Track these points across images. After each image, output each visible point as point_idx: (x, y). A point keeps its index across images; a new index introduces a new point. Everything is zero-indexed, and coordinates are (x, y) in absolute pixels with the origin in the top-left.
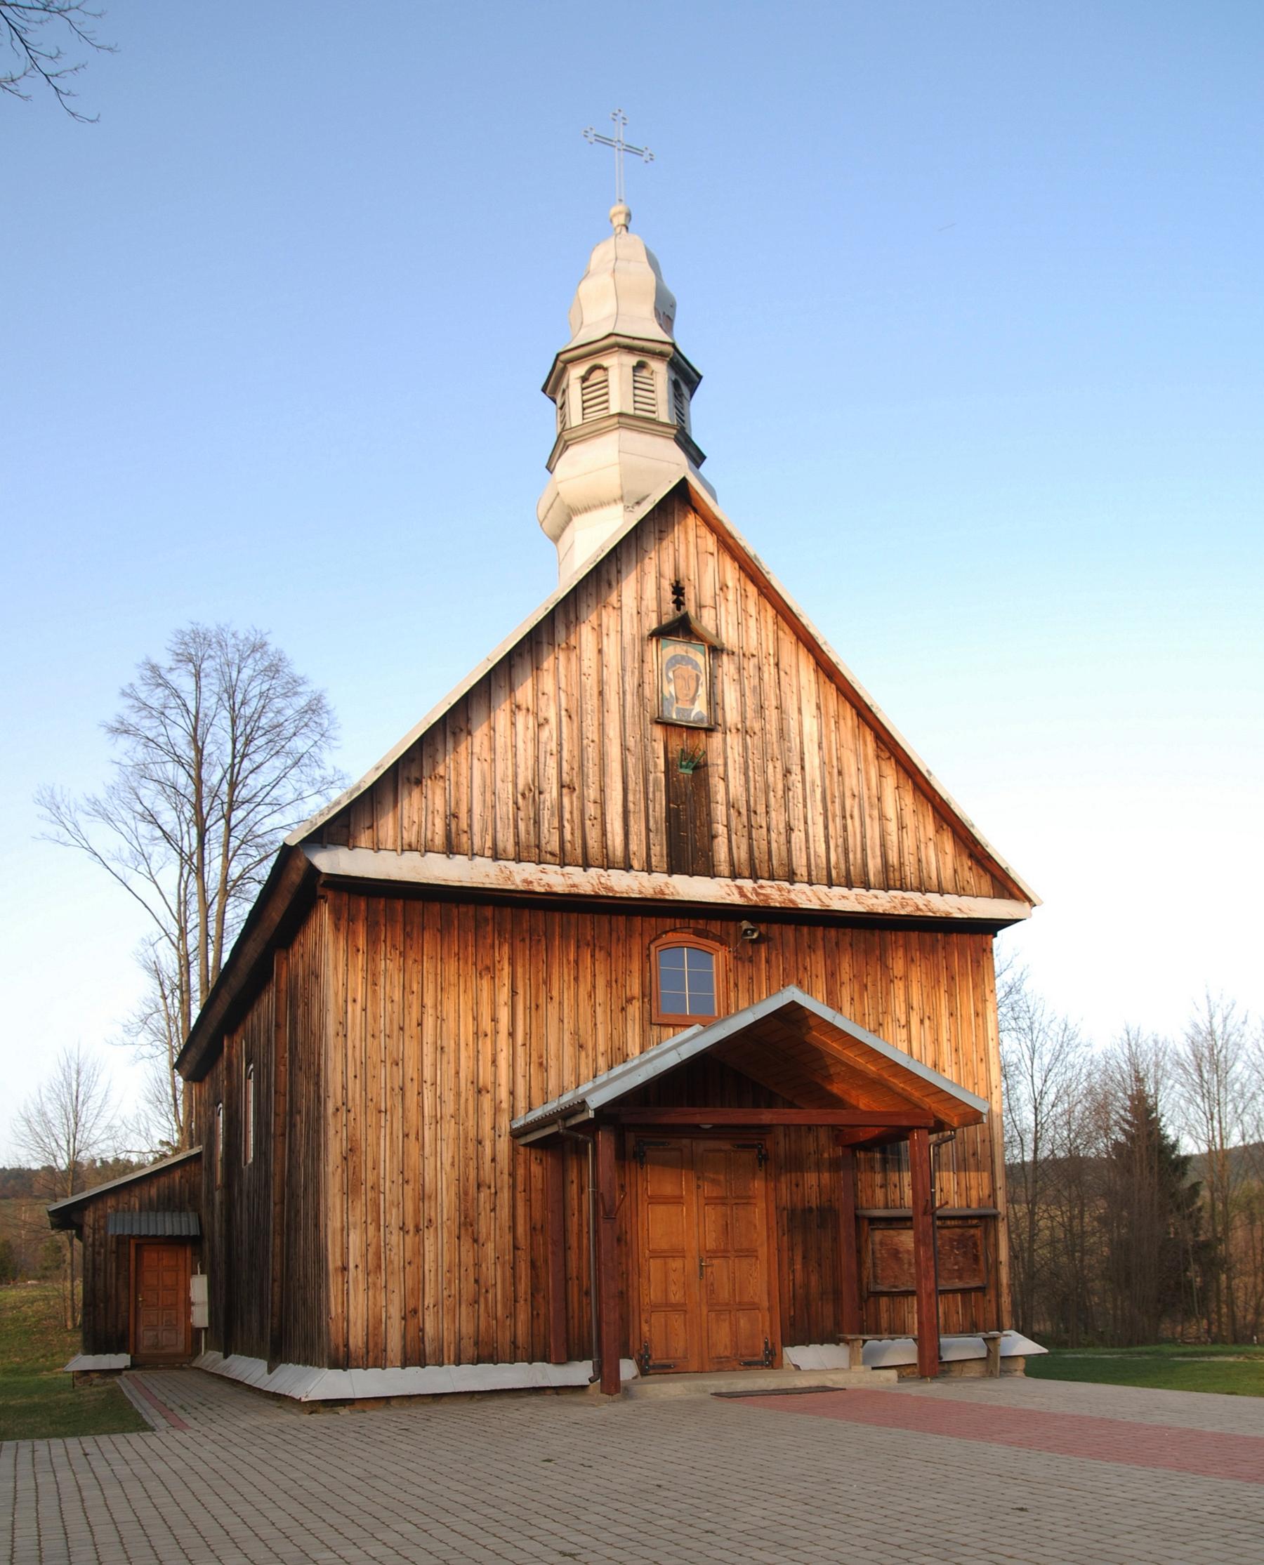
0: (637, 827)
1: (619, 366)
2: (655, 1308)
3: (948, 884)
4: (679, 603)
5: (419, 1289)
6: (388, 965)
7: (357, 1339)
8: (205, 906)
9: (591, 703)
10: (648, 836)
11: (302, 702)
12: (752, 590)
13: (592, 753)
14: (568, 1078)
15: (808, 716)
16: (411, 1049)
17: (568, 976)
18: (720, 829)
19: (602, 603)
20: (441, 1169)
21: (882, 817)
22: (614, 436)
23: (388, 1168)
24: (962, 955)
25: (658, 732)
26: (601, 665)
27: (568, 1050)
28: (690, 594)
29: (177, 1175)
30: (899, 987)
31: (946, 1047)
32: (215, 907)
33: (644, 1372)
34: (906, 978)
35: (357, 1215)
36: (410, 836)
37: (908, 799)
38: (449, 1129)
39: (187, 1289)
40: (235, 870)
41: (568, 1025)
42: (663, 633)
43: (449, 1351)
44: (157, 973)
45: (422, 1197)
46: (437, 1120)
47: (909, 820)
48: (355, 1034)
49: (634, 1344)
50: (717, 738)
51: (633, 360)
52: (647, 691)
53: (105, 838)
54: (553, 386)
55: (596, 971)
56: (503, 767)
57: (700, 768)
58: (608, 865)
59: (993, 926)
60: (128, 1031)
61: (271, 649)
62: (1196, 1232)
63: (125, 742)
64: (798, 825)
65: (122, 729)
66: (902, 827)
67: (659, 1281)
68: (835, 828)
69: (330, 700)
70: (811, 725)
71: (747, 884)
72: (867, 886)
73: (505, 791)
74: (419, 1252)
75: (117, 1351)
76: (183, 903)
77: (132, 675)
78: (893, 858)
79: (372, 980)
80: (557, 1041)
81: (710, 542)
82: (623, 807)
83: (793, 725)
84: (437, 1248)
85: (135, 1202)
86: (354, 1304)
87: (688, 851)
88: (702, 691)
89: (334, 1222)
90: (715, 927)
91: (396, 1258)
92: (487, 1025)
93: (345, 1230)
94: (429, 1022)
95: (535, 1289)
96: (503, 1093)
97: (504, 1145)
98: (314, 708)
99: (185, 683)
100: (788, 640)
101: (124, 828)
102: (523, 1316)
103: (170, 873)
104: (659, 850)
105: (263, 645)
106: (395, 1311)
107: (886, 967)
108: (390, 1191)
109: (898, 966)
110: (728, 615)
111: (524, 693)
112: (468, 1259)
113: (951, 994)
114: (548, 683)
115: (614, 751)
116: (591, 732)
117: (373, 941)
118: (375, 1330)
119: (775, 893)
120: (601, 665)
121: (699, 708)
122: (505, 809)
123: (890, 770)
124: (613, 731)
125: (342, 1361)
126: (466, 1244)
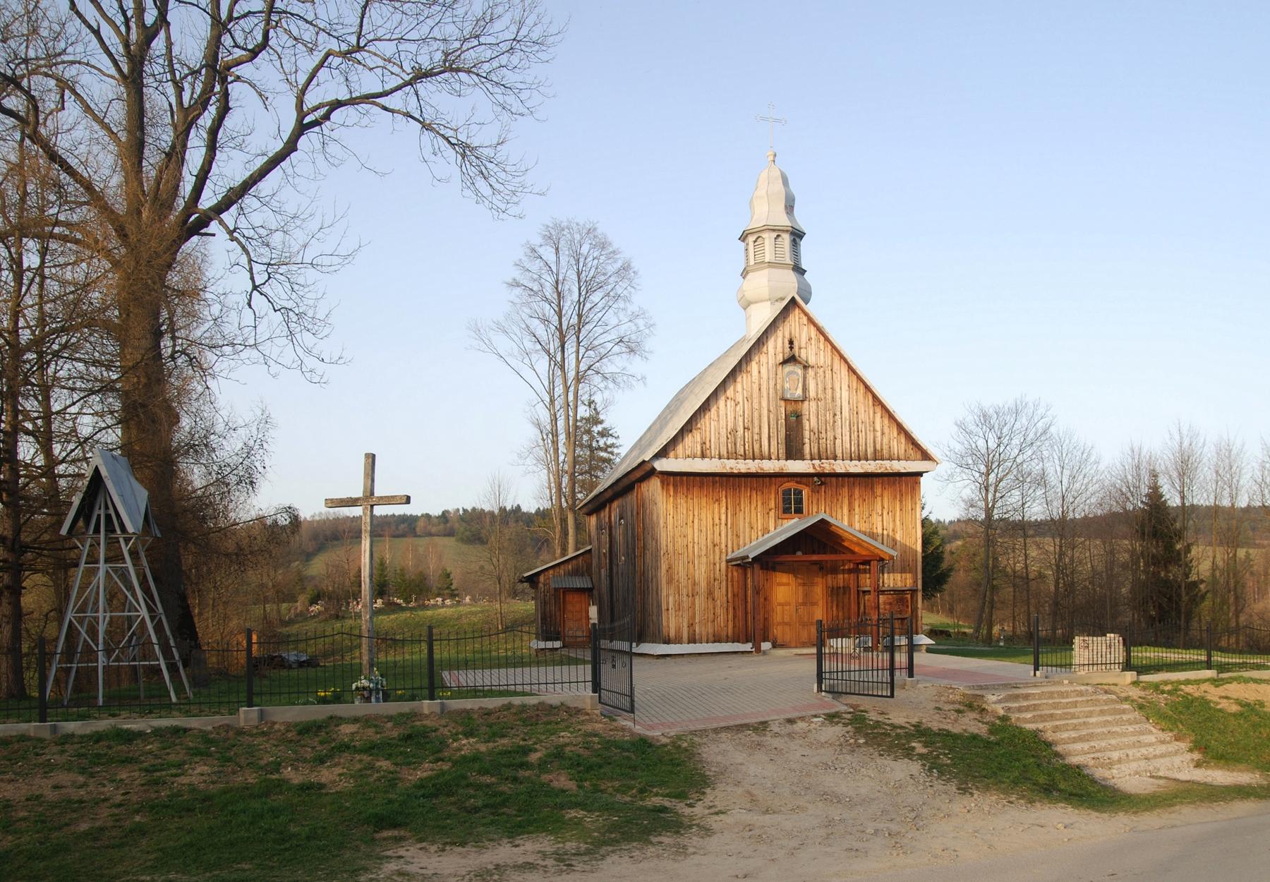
0: (774, 443)
1: (768, 238)
2: (779, 624)
3: (902, 456)
4: (791, 348)
5: (693, 617)
6: (681, 500)
7: (672, 634)
8: (567, 389)
9: (756, 394)
10: (778, 446)
11: (619, 264)
12: (822, 338)
13: (756, 414)
14: (747, 540)
15: (844, 392)
16: (690, 531)
17: (747, 502)
18: (807, 441)
19: (760, 351)
20: (701, 573)
21: (874, 430)
22: (766, 271)
23: (682, 574)
24: (907, 485)
25: (783, 403)
26: (760, 378)
27: (747, 530)
28: (796, 344)
29: (580, 559)
30: (879, 499)
31: (898, 523)
32: (572, 389)
33: (774, 646)
34: (882, 496)
35: (671, 592)
36: (688, 452)
37: (886, 421)
38: (704, 560)
39: (587, 612)
40: (583, 367)
41: (747, 520)
42: (785, 362)
43: (704, 639)
44: (538, 425)
45: (694, 584)
46: (699, 557)
47: (886, 430)
48: (670, 527)
49: (771, 637)
50: (806, 403)
51: (775, 234)
52: (779, 387)
53: (504, 344)
54: (743, 238)
55: (757, 499)
56: (723, 423)
57: (799, 416)
58: (762, 458)
59: (920, 474)
60: (520, 456)
61: (599, 231)
62: (1187, 576)
63: (518, 291)
64: (839, 436)
65: (515, 284)
66: (883, 434)
67: (778, 615)
68: (854, 436)
69: (635, 265)
70: (845, 394)
71: (817, 462)
72: (867, 460)
73: (723, 432)
74: (694, 604)
75: (557, 639)
76: (552, 382)
77: (520, 254)
78: (878, 447)
79: (676, 507)
80: (742, 525)
81: (805, 319)
82: (770, 435)
83: (838, 395)
84: (700, 602)
85: (562, 572)
86: (672, 622)
87: (793, 449)
88: (800, 385)
89: (664, 593)
90: (804, 480)
91: (685, 605)
92: (717, 521)
93: (668, 596)
94: (696, 521)
95: (734, 617)
96: (723, 546)
97: (724, 565)
98: (626, 268)
99: (548, 254)
100: (837, 358)
101: (515, 338)
102: (730, 626)
103: (543, 364)
104: (782, 451)
105: (595, 229)
106: (685, 625)
107: (873, 493)
108: (683, 582)
109: (878, 491)
110: (811, 352)
111: (730, 392)
112: (711, 606)
113: (901, 501)
114: (739, 387)
115: (765, 412)
116: (756, 406)
117: (676, 492)
118: (678, 630)
119: (828, 466)
120: (760, 378)
121: (799, 392)
122: (723, 439)
123: (878, 409)
124: (764, 404)
125: (667, 641)
126: (710, 601)
